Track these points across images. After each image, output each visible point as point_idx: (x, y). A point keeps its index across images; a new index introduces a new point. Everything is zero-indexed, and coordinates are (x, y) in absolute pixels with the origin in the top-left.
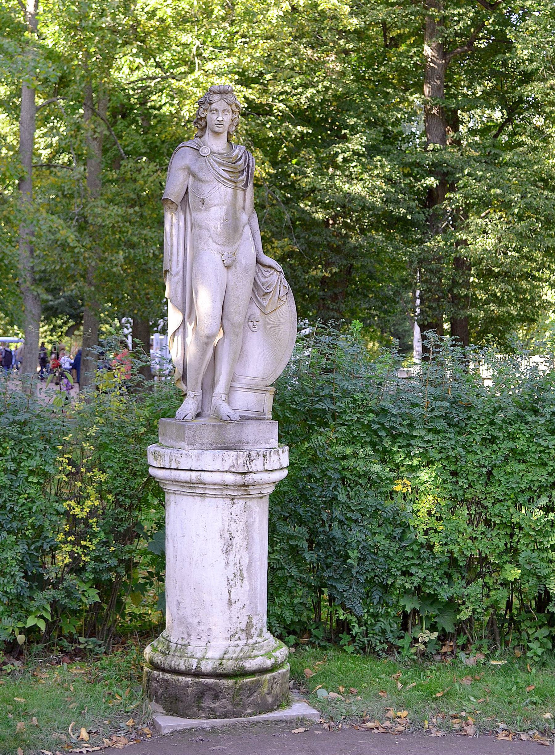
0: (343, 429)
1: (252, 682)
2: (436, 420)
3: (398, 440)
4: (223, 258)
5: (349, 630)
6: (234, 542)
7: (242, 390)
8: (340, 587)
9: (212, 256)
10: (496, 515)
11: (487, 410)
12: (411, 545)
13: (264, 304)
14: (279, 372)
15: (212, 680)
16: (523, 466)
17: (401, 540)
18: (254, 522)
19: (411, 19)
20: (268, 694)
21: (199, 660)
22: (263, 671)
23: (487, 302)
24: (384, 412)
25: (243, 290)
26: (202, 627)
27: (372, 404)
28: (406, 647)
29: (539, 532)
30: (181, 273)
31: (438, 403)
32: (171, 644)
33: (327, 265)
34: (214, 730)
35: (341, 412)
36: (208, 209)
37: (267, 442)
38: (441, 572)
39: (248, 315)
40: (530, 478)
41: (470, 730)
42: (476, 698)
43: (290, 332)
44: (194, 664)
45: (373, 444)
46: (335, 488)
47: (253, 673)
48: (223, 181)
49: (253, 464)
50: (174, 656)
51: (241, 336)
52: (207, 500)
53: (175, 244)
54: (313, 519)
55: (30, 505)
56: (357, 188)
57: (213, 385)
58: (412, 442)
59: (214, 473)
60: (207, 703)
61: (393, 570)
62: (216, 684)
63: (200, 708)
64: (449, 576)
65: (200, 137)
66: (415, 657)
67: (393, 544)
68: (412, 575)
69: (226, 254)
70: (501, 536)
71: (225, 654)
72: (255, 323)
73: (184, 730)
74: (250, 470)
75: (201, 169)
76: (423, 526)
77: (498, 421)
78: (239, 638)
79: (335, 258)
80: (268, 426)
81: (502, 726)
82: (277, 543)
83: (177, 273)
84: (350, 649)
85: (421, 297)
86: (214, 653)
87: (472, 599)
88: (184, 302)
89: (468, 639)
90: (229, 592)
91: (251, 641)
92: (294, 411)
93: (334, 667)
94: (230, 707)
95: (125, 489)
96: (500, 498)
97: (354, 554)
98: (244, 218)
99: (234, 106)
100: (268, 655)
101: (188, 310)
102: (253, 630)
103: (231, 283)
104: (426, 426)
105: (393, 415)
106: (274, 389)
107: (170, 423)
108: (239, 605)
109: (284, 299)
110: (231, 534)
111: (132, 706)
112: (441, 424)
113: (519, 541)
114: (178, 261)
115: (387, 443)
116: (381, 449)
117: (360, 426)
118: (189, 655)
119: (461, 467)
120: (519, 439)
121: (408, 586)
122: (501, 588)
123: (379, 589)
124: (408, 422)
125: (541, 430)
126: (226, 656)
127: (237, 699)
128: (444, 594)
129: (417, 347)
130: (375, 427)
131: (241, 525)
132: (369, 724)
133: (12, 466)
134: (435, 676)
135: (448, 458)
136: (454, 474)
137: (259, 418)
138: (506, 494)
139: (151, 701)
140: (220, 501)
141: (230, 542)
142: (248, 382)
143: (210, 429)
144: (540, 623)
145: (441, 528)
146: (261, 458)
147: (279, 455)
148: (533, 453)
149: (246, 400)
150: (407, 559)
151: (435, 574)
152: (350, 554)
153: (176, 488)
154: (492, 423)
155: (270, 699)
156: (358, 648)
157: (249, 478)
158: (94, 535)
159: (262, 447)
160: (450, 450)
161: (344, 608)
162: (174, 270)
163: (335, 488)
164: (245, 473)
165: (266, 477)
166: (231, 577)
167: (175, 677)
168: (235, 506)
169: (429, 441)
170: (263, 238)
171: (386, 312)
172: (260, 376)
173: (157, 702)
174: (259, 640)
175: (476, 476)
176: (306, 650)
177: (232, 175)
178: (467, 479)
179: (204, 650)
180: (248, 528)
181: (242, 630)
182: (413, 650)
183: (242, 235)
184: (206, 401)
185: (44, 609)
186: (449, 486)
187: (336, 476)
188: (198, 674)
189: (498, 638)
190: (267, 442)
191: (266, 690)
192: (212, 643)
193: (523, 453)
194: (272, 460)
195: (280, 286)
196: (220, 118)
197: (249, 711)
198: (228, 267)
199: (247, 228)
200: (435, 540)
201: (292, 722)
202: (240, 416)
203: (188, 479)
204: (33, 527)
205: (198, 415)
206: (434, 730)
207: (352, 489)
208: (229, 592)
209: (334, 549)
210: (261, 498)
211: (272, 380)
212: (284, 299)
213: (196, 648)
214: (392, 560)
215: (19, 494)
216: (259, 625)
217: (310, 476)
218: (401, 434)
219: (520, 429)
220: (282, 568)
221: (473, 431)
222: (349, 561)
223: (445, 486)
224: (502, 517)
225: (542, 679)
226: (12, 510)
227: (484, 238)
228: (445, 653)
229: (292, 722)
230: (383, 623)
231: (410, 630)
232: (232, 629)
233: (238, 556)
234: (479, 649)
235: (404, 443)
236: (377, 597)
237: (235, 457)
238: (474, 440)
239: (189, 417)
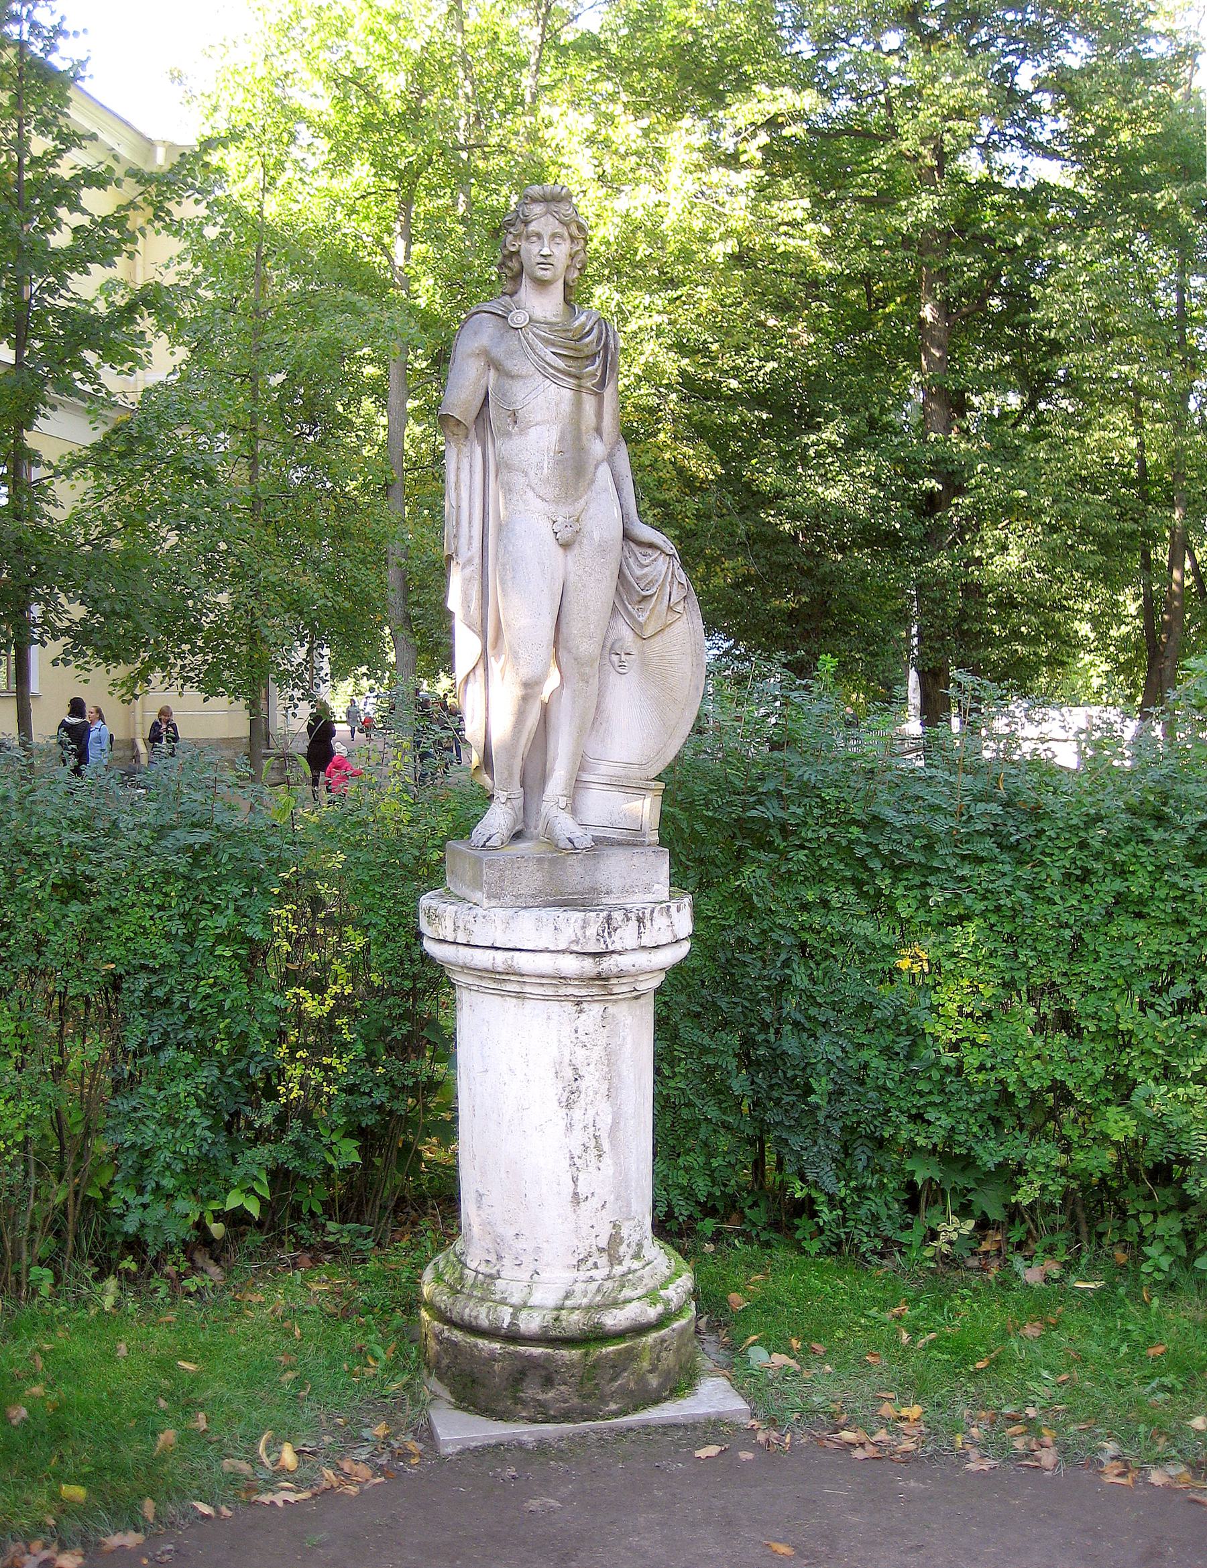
0: (802, 855)
1: (619, 1352)
2: (976, 838)
3: (905, 876)
5: (814, 1214)
6: (583, 1084)
8: (796, 1142)
9: (532, 519)
10: (1088, 1016)
11: (1073, 822)
12: (928, 1068)
14: (670, 756)
15: (540, 1350)
16: (1140, 926)
17: (909, 1057)
18: (621, 1046)
20: (650, 1372)
21: (517, 1309)
22: (640, 1330)
23: (1007, 640)
24: (876, 823)
25: (595, 591)
26: (520, 1245)
27: (857, 812)
28: (916, 1244)
29: (1171, 1050)
30: (477, 561)
31: (981, 806)
32: (467, 1271)
33: (798, 592)
34: (543, 1448)
35: (797, 825)
36: (522, 432)
37: (647, 889)
38: (982, 1116)
40: (1155, 947)
41: (1048, 1457)
42: (1052, 1371)
43: (693, 673)
44: (505, 1316)
45: (858, 883)
46: (786, 964)
47: (620, 1335)
49: (616, 937)
50: (470, 1296)
51: (595, 682)
52: (529, 1004)
53: (465, 505)
54: (746, 1017)
55: (221, 997)
56: (833, 494)
57: (544, 778)
58: (930, 879)
60: (532, 1391)
61: (893, 1113)
62: (548, 1358)
63: (517, 1400)
64: (997, 1122)
65: (511, 295)
66: (933, 1265)
67: (893, 1066)
68: (929, 1123)
69: (560, 519)
70: (1096, 1054)
71: (567, 1297)
73: (484, 1447)
74: (611, 948)
75: (510, 353)
76: (949, 1034)
77: (1096, 844)
78: (595, 1264)
79: (806, 583)
80: (650, 859)
81: (1111, 1448)
82: (680, 1059)
83: (469, 561)
84: (813, 1247)
85: (919, 635)
86: (546, 1296)
87: (1041, 1169)
88: (484, 620)
89: (1029, 1232)
90: (575, 1181)
91: (619, 1270)
92: (710, 822)
93: (782, 1285)
94: (576, 1400)
95: (401, 963)
96: (1097, 985)
97: (822, 1085)
98: (598, 448)
100: (651, 1296)
101: (490, 633)
102: (623, 1249)
103: (572, 579)
104: (957, 851)
105: (895, 829)
106: (662, 785)
107: (461, 851)
108: (594, 1203)
109: (679, 608)
110: (576, 1069)
111: (394, 1386)
112: (986, 847)
113: (1130, 1063)
114: (471, 537)
115: (884, 883)
116: (872, 892)
117: (833, 851)
118: (497, 1297)
119: (1024, 927)
120: (1133, 873)
121: (920, 1141)
122: (1095, 1147)
123: (866, 1142)
124: (925, 841)
125: (1175, 857)
126: (568, 1303)
127: (590, 1385)
128: (989, 1155)
129: (914, 698)
130: (861, 852)
131: (597, 1053)
132: (847, 1435)
133: (178, 927)
134: (968, 1313)
135: (998, 909)
136: (1010, 939)
137: (631, 841)
138: (1108, 978)
139: (430, 1374)
140: (554, 1006)
141: (575, 1085)
143: (532, 867)
144: (1164, 1207)
145: (984, 1037)
146: (633, 923)
147: (669, 916)
148: (1162, 900)
150: (921, 1094)
151: (972, 1121)
152: (815, 1085)
153: (470, 980)
154: (1083, 845)
155: (654, 1381)
156: (827, 1244)
157: (608, 964)
158: (345, 1047)
159: (636, 901)
160: (1003, 895)
161: (803, 1178)
163: (786, 964)
166: (578, 1151)
167: (472, 1340)
168: (583, 1016)
169: (963, 879)
171: (873, 655)
173: (440, 1379)
174: (636, 1265)
175: (1053, 943)
176: (735, 1247)
177: (571, 363)
178: (1035, 949)
179: (527, 1290)
180: (610, 1057)
181: (601, 1250)
182: (928, 1253)
183: (593, 481)
184: (532, 809)
185: (256, 1179)
186: (999, 962)
187: (787, 940)
188: (513, 1337)
189: (1084, 1229)
190: (647, 889)
191: (646, 1365)
192: (543, 1275)
193: (1141, 901)
194: (656, 927)
195: (672, 583)
196: (546, 251)
197: (613, 1407)
198: (566, 546)
199: (604, 469)
200: (972, 1060)
201: (695, 1428)
203: (489, 965)
204: (229, 1035)
205: (517, 836)
206: (974, 1454)
207: (818, 964)
208: (575, 1181)
209: (785, 1073)
210: (637, 998)
212: (679, 608)
213: (512, 1285)
214: (892, 1094)
215: (199, 979)
216: (636, 1237)
217: (741, 941)
218: (909, 865)
219: (1135, 856)
220: (689, 1105)
221: (1047, 859)
222: (812, 1099)
223: (992, 961)
224: (1100, 1020)
225: (1177, 1320)
226: (184, 1007)
227: (1009, 556)
228: (986, 1253)
229: (695, 1428)
230: (874, 1204)
231: (923, 1213)
232: (581, 1250)
234: (1050, 1250)
235: (917, 880)
236: (864, 1157)
237: (580, 923)
238: (1048, 876)
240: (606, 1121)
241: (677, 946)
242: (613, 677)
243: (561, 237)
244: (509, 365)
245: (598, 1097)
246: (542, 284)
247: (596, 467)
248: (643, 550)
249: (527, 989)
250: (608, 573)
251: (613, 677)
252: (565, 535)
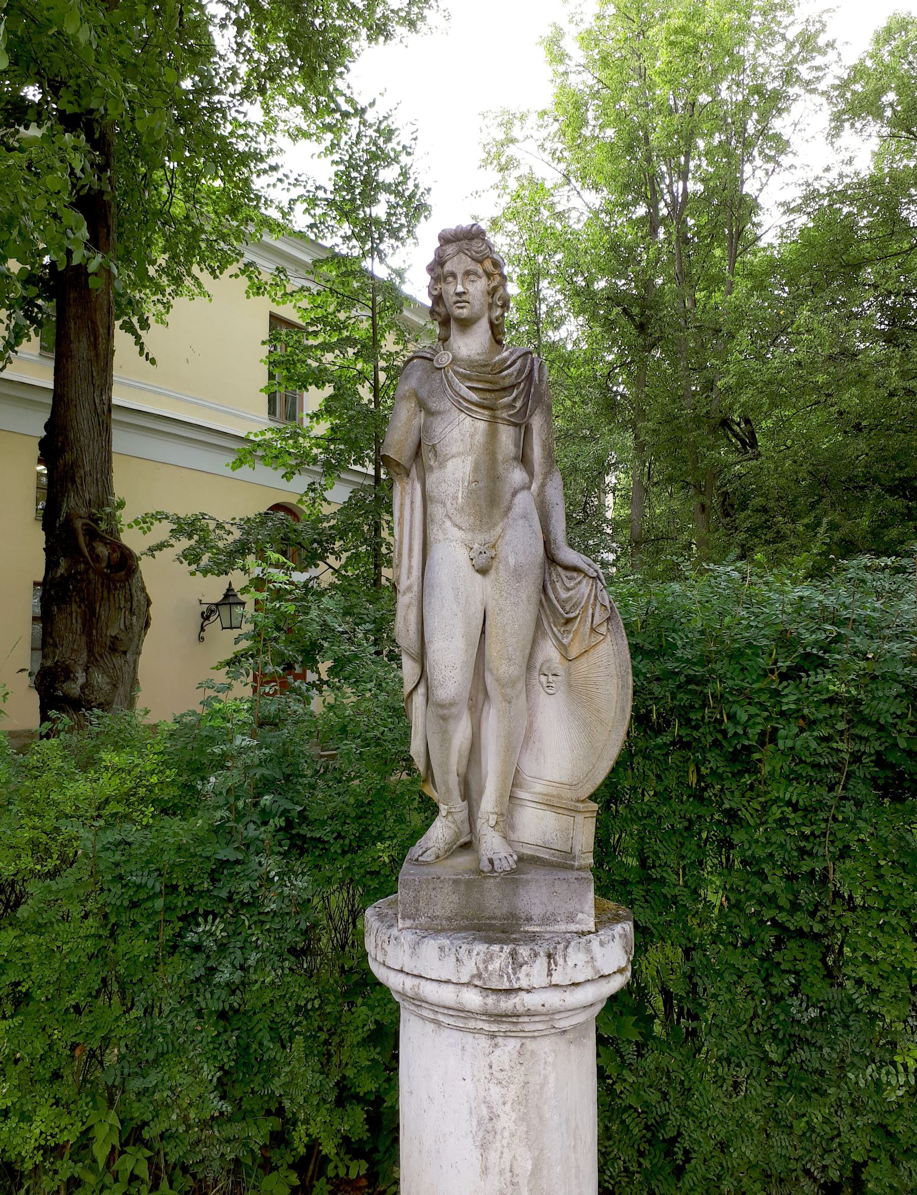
6: (499, 1125)
7: (534, 805)
9: (453, 551)
13: (565, 641)
30: (416, 588)
37: (571, 918)
43: (619, 695)
48: (467, 408)
49: (522, 974)
69: (476, 546)
74: (516, 986)
75: (431, 393)
83: (409, 588)
114: (410, 567)
131: (513, 1091)
142: (545, 790)
143: (448, 888)
149: (537, 826)
164: (508, 991)
165: (553, 999)
168: (498, 1052)
172: (565, 780)
177: (488, 395)
183: (509, 509)
190: (571, 918)
194: (570, 963)
195: (594, 605)
196: (460, 289)
198: (483, 571)
211: (590, 789)
233: (507, 1156)
240: (526, 1165)
241: (603, 982)
243: (475, 274)
244: (434, 405)
245: (516, 1140)
247: (514, 494)
248: (569, 574)
250: (524, 597)
252: (481, 561)
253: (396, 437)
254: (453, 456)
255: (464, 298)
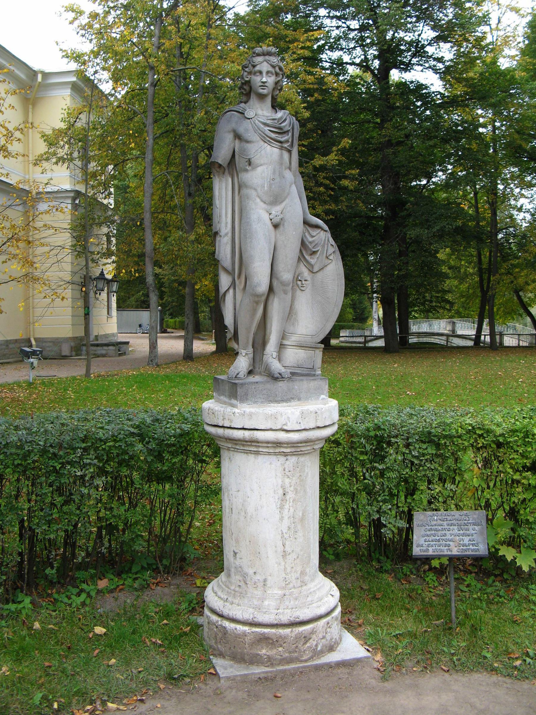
4: (271, 217)
6: (288, 497)
15: (269, 630)
19: (135, 271)
26: (258, 577)
30: (230, 235)
36: (254, 169)
39: (297, 274)
57: (264, 344)
59: (266, 432)
72: (304, 282)
83: (226, 234)
99: (277, 69)
109: (331, 257)
114: (227, 223)
140: (273, 458)
162: (223, 232)
168: (288, 462)
170: (307, 196)
184: (258, 358)
196: (264, 80)
198: (276, 226)
202: (291, 373)
205: (250, 372)
212: (331, 257)
239: (241, 375)
242: (298, 292)
243: (272, 73)
246: (262, 97)
247: (290, 186)
249: (261, 449)
251: (298, 292)
252: (276, 220)
253: (223, 152)
254: (261, 165)
255: (266, 84)
